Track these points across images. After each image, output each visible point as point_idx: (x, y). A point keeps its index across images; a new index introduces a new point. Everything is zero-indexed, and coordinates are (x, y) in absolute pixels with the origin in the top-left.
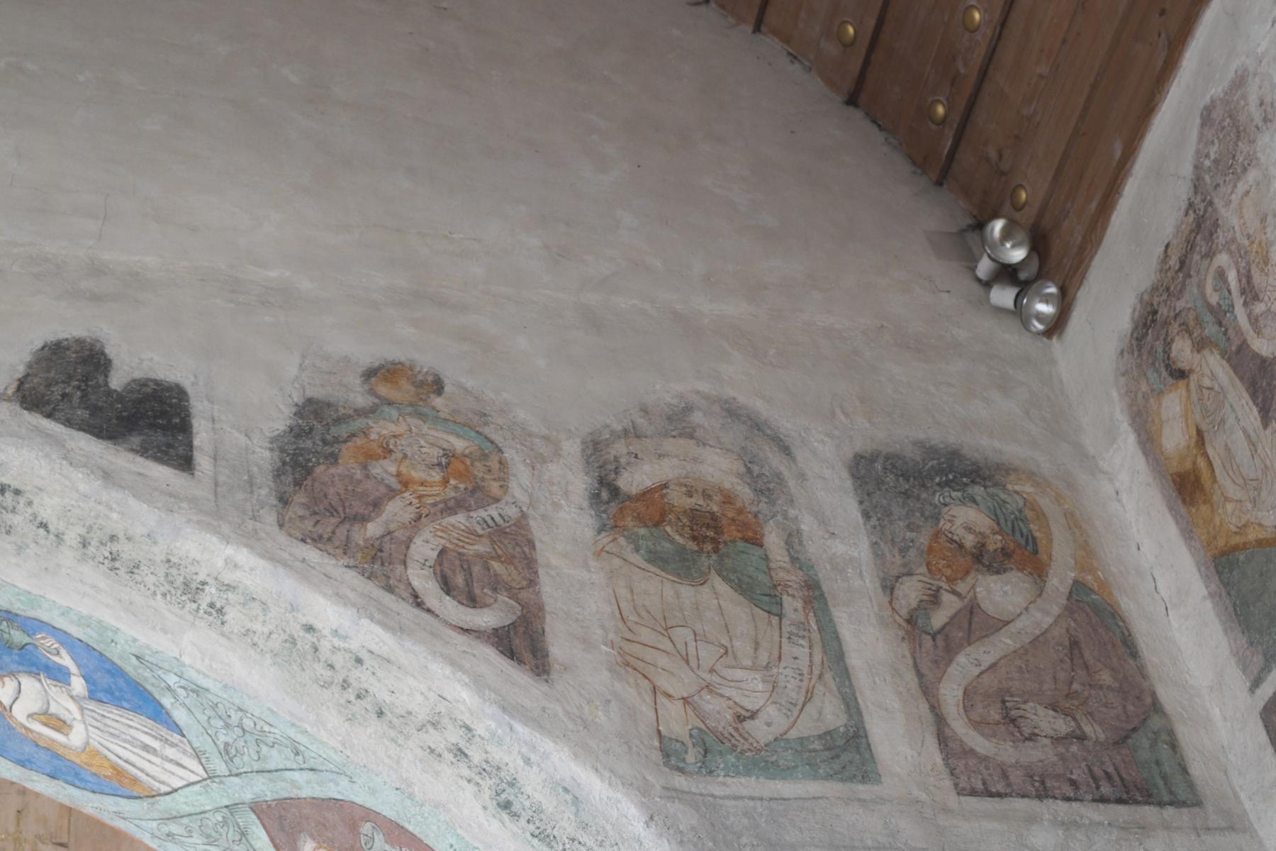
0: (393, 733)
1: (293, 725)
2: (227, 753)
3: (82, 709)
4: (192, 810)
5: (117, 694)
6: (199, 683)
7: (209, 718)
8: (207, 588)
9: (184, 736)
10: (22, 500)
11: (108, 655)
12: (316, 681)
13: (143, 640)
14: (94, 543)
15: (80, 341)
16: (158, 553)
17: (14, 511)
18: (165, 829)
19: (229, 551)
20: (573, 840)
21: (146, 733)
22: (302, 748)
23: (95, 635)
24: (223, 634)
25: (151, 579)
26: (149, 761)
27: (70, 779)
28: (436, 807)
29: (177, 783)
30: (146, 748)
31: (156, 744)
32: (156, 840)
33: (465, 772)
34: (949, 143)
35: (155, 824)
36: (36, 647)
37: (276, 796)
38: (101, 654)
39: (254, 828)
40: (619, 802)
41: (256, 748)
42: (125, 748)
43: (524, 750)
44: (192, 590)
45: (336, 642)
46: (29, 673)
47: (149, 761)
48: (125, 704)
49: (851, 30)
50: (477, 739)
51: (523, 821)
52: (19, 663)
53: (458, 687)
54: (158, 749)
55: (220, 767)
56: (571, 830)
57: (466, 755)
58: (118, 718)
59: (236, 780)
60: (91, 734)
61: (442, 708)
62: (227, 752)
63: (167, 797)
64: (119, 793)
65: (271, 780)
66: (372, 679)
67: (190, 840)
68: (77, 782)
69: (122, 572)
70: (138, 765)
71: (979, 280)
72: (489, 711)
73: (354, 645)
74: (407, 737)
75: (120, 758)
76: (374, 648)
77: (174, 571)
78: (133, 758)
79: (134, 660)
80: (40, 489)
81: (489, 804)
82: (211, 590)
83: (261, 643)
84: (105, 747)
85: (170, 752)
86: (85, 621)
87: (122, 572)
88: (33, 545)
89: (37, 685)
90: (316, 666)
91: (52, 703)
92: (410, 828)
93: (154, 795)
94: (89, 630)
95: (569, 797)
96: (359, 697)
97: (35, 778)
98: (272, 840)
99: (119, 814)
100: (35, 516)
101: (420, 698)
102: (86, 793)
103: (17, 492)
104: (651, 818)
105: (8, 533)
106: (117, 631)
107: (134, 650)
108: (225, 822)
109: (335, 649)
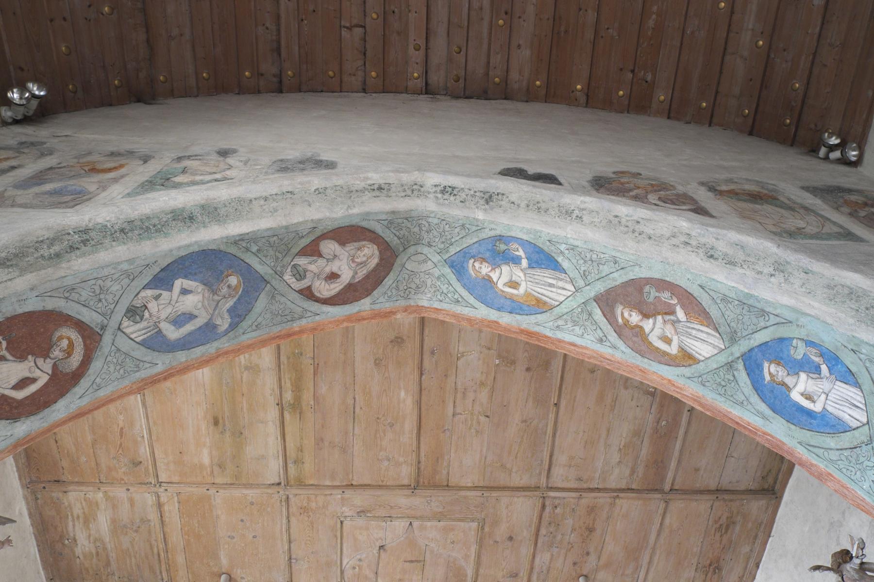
0: (656, 243)
1: (614, 249)
2: (584, 275)
3: (525, 274)
4: (568, 310)
5: (540, 262)
6: (574, 244)
7: (578, 260)
8: (574, 211)
9: (566, 274)
10: (505, 197)
11: (537, 244)
12: (622, 232)
13: (552, 232)
14: (531, 205)
15: (515, 168)
16: (555, 204)
17: (502, 200)
18: (556, 324)
19: (582, 198)
20: (745, 261)
21: (551, 278)
22: (618, 259)
23: (532, 236)
24: (583, 225)
25: (553, 213)
26: (551, 291)
27: (517, 311)
28: (680, 264)
29: (562, 298)
30: (551, 285)
31: (554, 282)
32: (552, 332)
33: (691, 249)
34: (794, 130)
35: (552, 323)
36: (509, 250)
37: (605, 289)
38: (535, 245)
39: (595, 310)
40: (763, 243)
41: (598, 268)
42: (542, 288)
43: (715, 236)
44: (569, 213)
45: (628, 218)
46: (505, 263)
47: (551, 291)
48: (543, 266)
49: (747, 111)
50: (693, 237)
51: (720, 260)
52: (502, 260)
53: (681, 222)
54: (555, 284)
55: (581, 283)
56: (743, 258)
57: (689, 244)
58: (540, 274)
59: (588, 287)
60: (528, 286)
61: (676, 230)
62: (584, 276)
63: (558, 308)
64: (538, 312)
65: (604, 281)
66: (644, 227)
67: (566, 326)
68: (521, 312)
69: (542, 212)
70: (546, 295)
71: (821, 158)
72: (696, 227)
73: (635, 218)
74: (663, 243)
75: (539, 293)
76: (644, 217)
77: (562, 209)
78: (545, 292)
79: (548, 243)
80: (511, 193)
81: (703, 258)
82: (577, 212)
83: (598, 225)
84: (535, 291)
85: (561, 284)
86: (529, 232)
87: (542, 212)
88: (509, 209)
89: (508, 268)
90: (621, 227)
91: (514, 276)
92: (668, 279)
93: (552, 308)
94: (531, 235)
95: (738, 247)
96: (640, 234)
97: (503, 315)
98: (603, 313)
99: (537, 324)
100: (509, 201)
101: (666, 229)
102: (524, 316)
103: (503, 194)
104: (779, 246)
105: (500, 207)
106: (541, 232)
107: (548, 238)
108: (582, 311)
109: (627, 221)
